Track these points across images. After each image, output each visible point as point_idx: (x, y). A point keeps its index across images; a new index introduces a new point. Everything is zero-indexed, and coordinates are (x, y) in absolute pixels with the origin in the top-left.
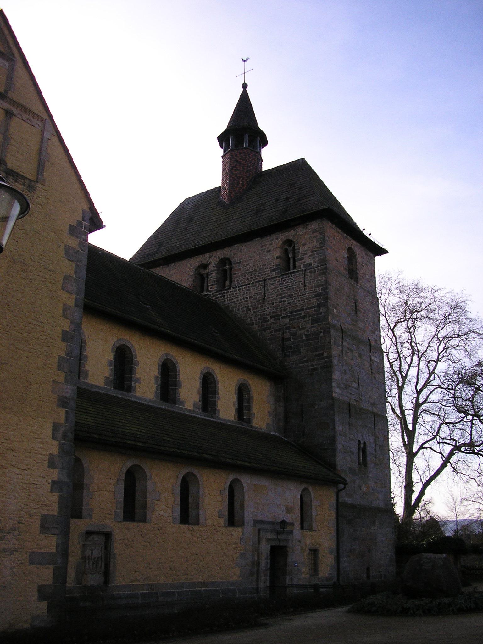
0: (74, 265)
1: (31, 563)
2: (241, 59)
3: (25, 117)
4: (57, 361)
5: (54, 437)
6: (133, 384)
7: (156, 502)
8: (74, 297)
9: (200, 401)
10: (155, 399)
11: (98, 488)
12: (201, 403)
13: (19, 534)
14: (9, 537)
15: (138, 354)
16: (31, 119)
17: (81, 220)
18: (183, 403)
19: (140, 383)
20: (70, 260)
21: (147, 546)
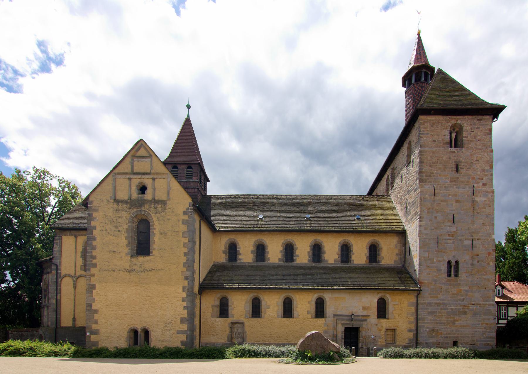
0: (187, 226)
1: (177, 333)
2: (417, 31)
3: (160, 176)
4: (182, 264)
5: (183, 291)
6: (295, 258)
7: (267, 309)
8: (188, 239)
9: (339, 258)
10: (308, 262)
11: (236, 306)
12: (340, 259)
13: (172, 325)
14: (169, 325)
15: (296, 244)
16: (163, 176)
17: (188, 207)
18: (327, 261)
19: (299, 257)
20: (185, 225)
21: (263, 328)
